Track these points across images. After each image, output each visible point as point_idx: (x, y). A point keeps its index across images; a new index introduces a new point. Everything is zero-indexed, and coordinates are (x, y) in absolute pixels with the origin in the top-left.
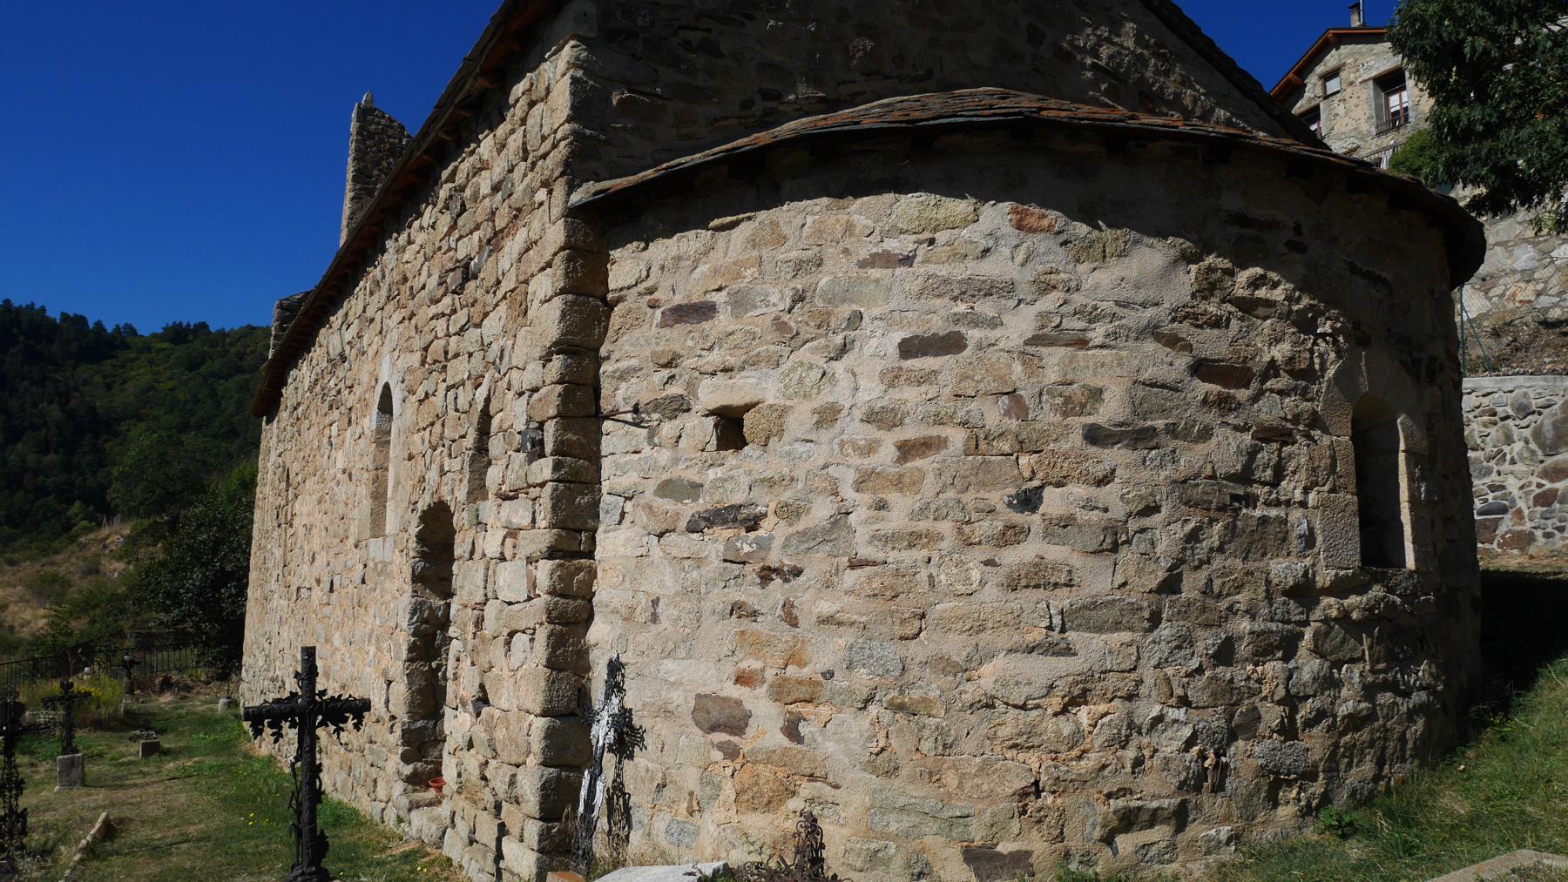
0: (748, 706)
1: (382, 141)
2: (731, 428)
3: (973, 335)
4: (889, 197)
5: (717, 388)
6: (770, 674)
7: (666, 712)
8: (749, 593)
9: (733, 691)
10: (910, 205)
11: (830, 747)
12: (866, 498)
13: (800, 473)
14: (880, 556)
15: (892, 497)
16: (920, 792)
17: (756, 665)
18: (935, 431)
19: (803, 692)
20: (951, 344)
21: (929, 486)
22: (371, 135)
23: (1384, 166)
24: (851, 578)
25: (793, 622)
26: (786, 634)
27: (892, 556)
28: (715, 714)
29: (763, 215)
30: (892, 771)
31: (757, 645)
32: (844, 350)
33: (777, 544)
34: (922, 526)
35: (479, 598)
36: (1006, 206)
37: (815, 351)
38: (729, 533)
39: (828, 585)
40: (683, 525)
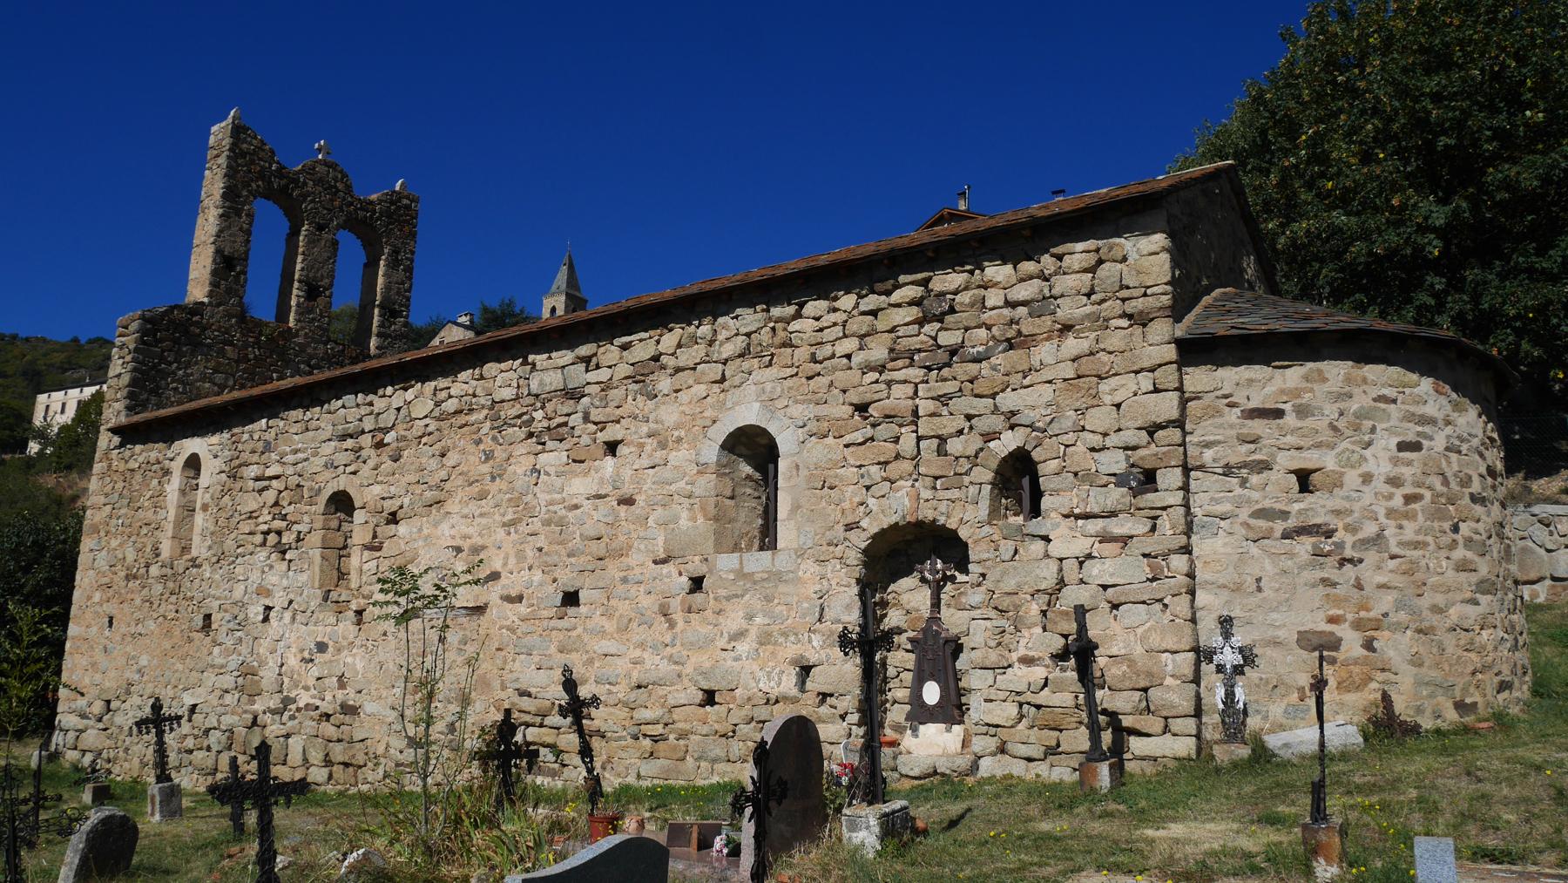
0: (1339, 634)
1: (252, 162)
2: (1304, 480)
3: (1426, 443)
4: (1383, 367)
5: (1293, 458)
6: (1350, 617)
7: (1276, 643)
8: (1330, 572)
9: (1324, 627)
10: (1395, 372)
11: (1391, 653)
12: (1392, 523)
13: (1357, 507)
14: (1402, 553)
15: (1405, 523)
16: (1434, 673)
17: (1340, 612)
18: (1418, 490)
19: (1373, 624)
20: (1415, 447)
21: (1420, 517)
22: (243, 154)
23: (560, 312)
24: (1392, 564)
25: (1362, 589)
26: (1355, 593)
27: (1408, 553)
28: (1315, 641)
29: (1310, 365)
30: (1421, 665)
31: (1337, 601)
32: (1369, 444)
33: (1348, 546)
34: (1420, 538)
35: (1049, 582)
36: (1431, 380)
37: (1353, 443)
38: (1314, 539)
39: (1379, 568)
40: (1278, 534)
